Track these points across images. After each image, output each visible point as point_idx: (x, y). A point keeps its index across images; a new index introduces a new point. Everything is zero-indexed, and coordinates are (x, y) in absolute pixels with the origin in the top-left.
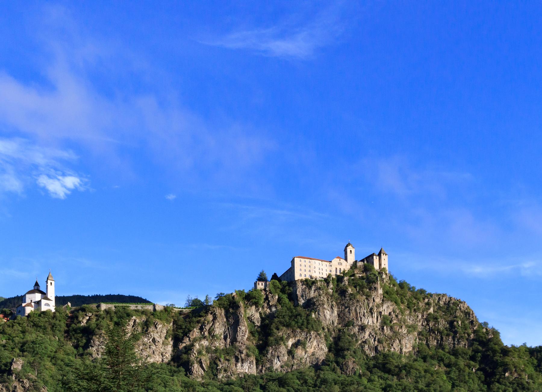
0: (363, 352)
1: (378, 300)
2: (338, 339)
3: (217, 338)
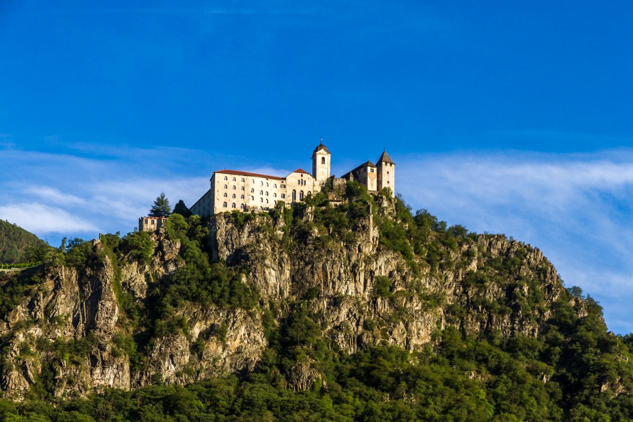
0: (336, 348)
1: (368, 250)
2: (288, 322)
3: (60, 323)
